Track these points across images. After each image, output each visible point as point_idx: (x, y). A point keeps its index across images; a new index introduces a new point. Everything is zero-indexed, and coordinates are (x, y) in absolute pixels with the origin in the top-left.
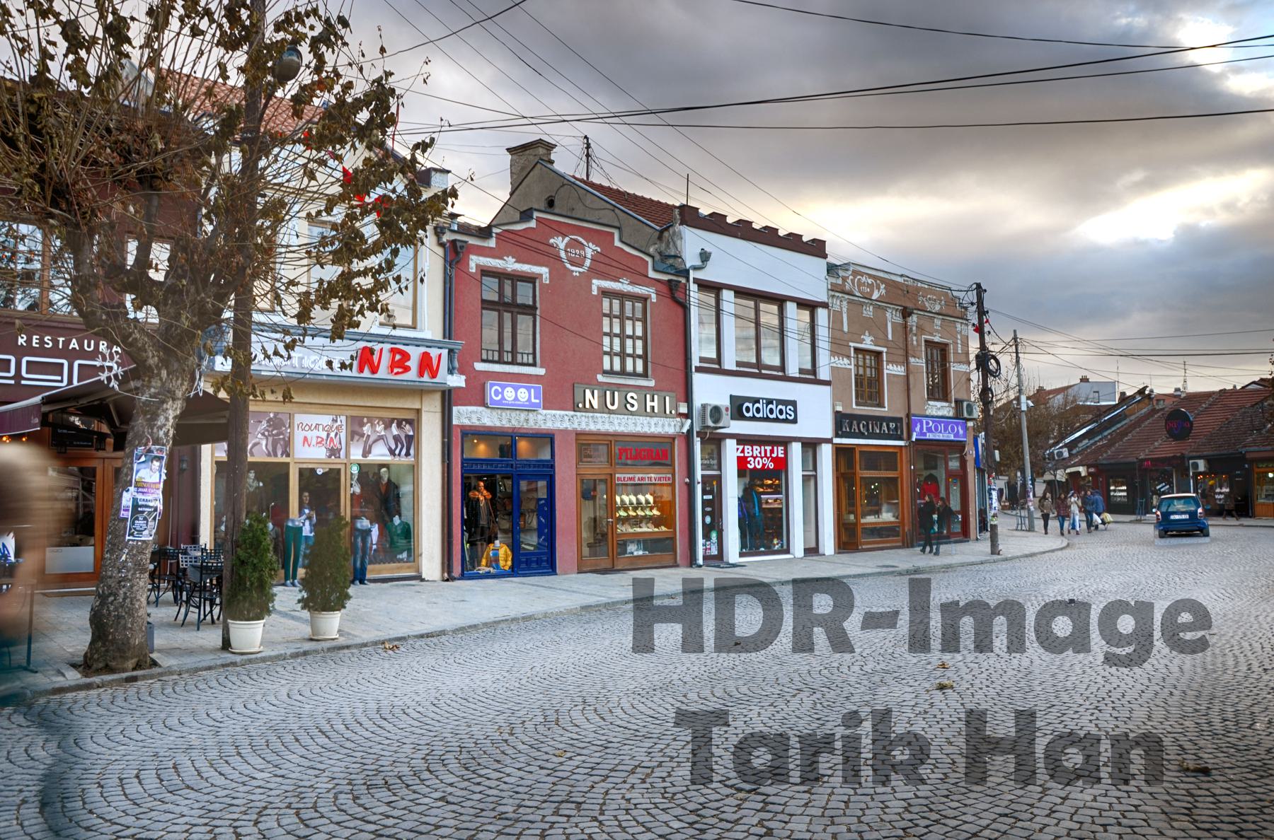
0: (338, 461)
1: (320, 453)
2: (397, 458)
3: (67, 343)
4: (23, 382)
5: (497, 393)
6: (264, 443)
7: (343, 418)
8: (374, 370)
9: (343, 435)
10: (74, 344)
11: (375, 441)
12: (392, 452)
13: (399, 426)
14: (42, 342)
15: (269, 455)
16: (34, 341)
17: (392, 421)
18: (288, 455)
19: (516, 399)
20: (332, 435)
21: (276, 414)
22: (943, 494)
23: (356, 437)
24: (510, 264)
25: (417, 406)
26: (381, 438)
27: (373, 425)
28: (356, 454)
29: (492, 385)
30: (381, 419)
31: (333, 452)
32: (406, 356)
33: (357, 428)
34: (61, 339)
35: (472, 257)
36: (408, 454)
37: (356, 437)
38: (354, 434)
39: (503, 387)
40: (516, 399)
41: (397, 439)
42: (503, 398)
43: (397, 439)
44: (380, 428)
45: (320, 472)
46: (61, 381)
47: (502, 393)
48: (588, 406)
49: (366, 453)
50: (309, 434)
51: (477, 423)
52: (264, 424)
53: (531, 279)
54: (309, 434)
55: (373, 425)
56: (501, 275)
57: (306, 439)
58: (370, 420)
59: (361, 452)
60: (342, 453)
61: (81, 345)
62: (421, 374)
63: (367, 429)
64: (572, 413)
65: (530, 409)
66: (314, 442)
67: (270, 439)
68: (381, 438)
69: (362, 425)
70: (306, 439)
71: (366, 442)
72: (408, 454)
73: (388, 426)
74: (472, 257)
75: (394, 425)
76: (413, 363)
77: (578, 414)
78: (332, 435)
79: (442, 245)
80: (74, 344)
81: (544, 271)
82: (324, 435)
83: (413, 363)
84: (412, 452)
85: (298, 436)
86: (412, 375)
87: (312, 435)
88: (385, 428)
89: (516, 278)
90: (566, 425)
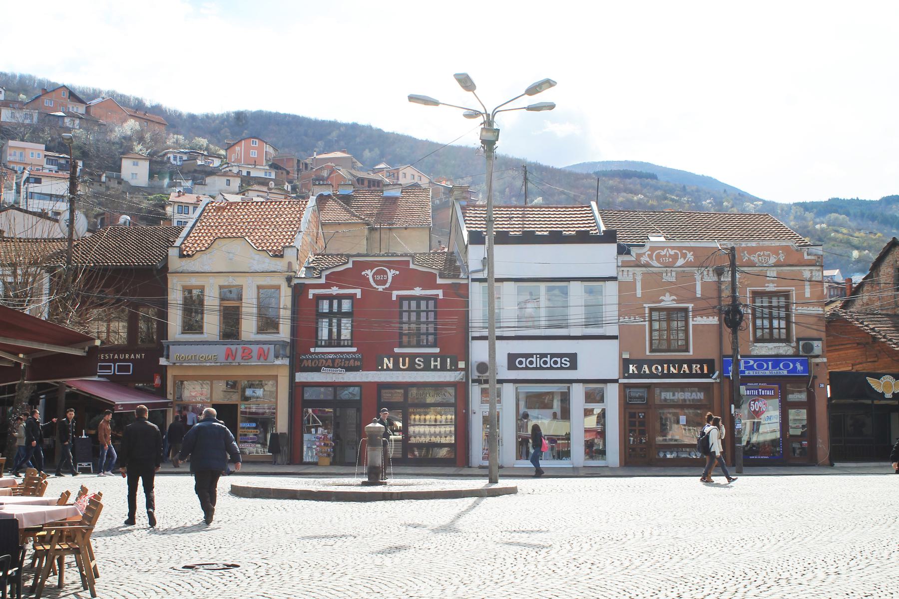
10: (116, 357)
79: (289, 286)
81: (358, 292)
83: (255, 354)
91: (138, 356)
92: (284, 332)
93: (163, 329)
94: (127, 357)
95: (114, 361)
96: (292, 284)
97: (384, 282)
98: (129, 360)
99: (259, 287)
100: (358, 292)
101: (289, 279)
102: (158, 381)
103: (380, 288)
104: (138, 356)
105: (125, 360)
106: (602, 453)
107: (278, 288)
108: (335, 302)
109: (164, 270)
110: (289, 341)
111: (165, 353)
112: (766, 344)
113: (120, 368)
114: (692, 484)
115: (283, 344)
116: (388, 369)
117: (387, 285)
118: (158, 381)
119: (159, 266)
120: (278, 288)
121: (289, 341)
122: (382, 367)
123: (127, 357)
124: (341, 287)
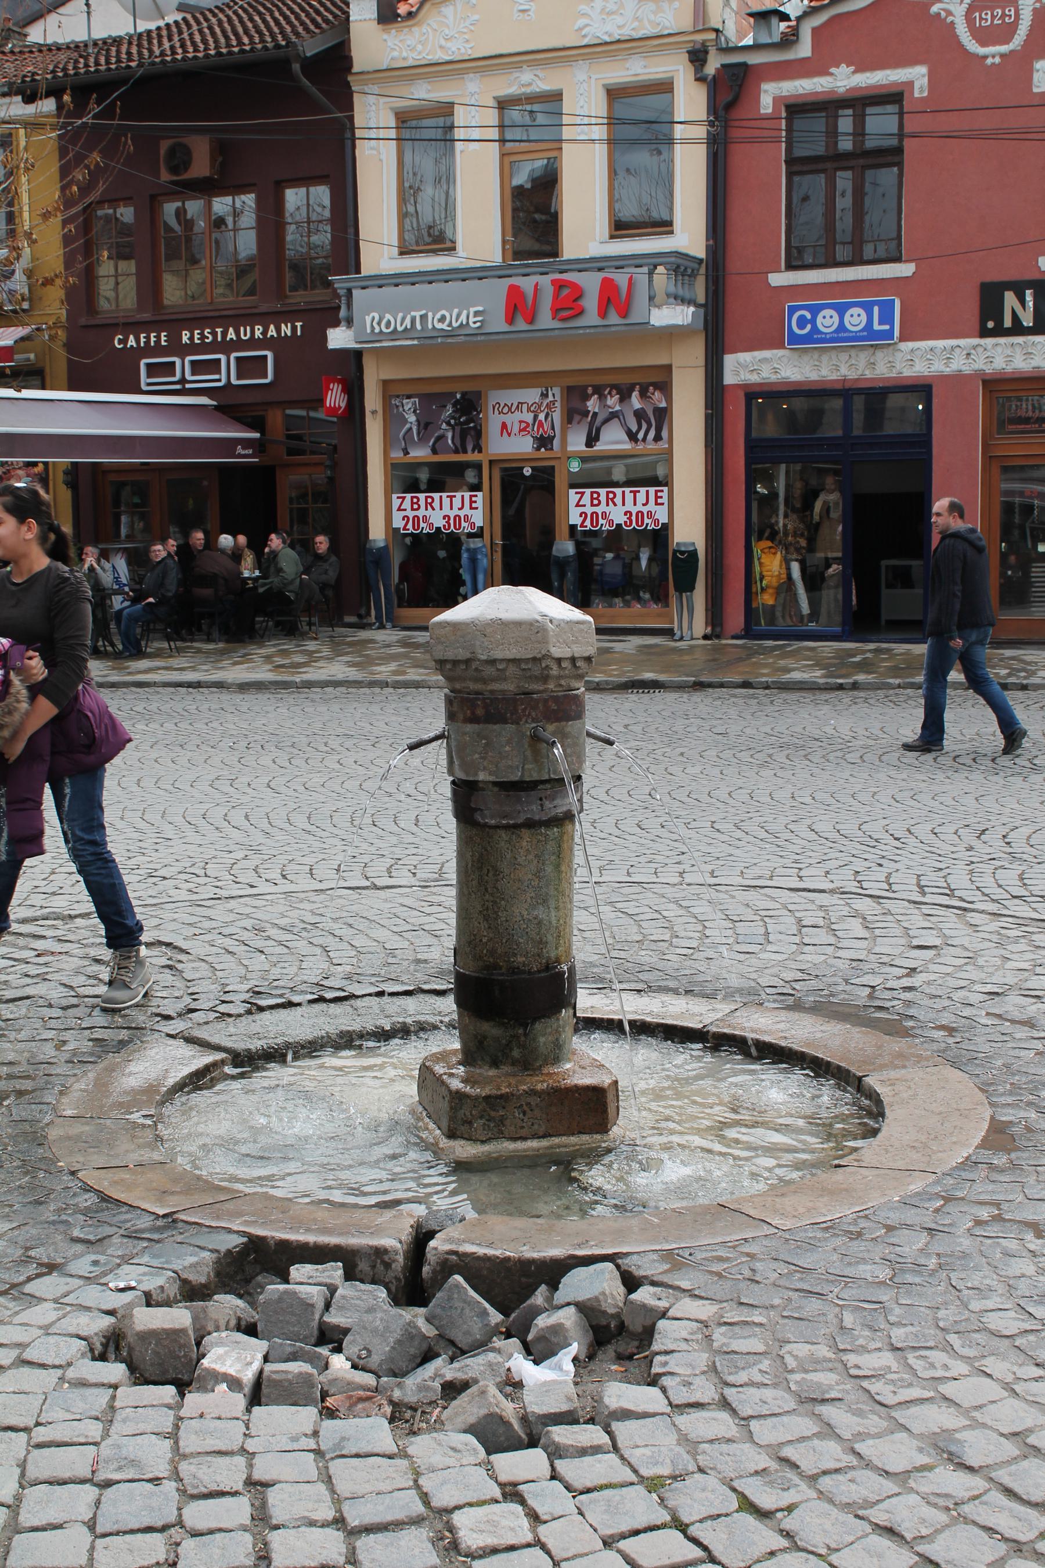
0: (549, 454)
1: (522, 446)
2: (640, 446)
3: (225, 334)
4: (187, 386)
5: (802, 322)
6: (450, 435)
7: (557, 391)
8: (531, 319)
9: (557, 416)
10: (231, 335)
11: (606, 421)
12: (632, 436)
13: (644, 395)
14: (203, 337)
15: (456, 451)
16: (163, 339)
17: (631, 389)
18: (480, 451)
19: (842, 327)
20: (542, 417)
21: (464, 394)
22: (795, 567)
23: (577, 418)
24: (844, 79)
25: (664, 361)
26: (614, 415)
27: (602, 397)
28: (577, 442)
29: (793, 310)
30: (613, 387)
31: (544, 442)
32: (578, 293)
33: (576, 404)
34: (219, 330)
35: (765, 86)
36: (658, 438)
37: (577, 418)
38: (573, 413)
39: (815, 310)
40: (842, 327)
41: (640, 415)
42: (815, 330)
43: (640, 415)
44: (613, 401)
45: (527, 472)
46: (219, 380)
47: (813, 321)
48: (1008, 323)
49: (592, 440)
50: (509, 419)
51: (774, 378)
52: (450, 410)
53: (893, 97)
54: (509, 419)
55: (602, 397)
56: (828, 107)
57: (504, 426)
58: (599, 390)
59: (583, 439)
60: (556, 443)
61: (237, 333)
62: (603, 313)
63: (592, 404)
64: (976, 341)
65: (872, 339)
66: (516, 429)
67: (458, 429)
68: (614, 415)
69: (587, 398)
70: (504, 426)
71: (591, 424)
72: (658, 438)
73: (625, 396)
74: (765, 86)
75: (635, 394)
76: (591, 302)
77: (989, 341)
78: (542, 417)
79: (700, 79)
80: (231, 335)
81: (916, 76)
82: (529, 417)
83: (591, 302)
84: (665, 434)
85: (493, 421)
86: (591, 317)
87: (513, 420)
88: (622, 400)
89: (861, 103)
90: (959, 364)
91: (286, 330)
92: (689, 235)
93: (346, 249)
94: (258, 334)
95: (226, 347)
96: (712, 67)
97: (1007, 32)
98: (265, 343)
99: (614, 94)
100: (916, 76)
101: (698, 57)
102: (335, 397)
103: (993, 53)
104: (286, 330)
105: (253, 343)
106: (404, 119)
107: (665, 87)
108: (845, 123)
109: (334, 66)
110: (701, 254)
111: (343, 313)
112: (311, 1238)
113: (245, 366)
114: (61, 41)
115: (681, 266)
116: (1018, 329)
117: (1017, 41)
118: (335, 397)
119: (311, 47)
120: (665, 87)
121: (701, 254)
122: (999, 321)
123: (258, 334)
124: (861, 68)
